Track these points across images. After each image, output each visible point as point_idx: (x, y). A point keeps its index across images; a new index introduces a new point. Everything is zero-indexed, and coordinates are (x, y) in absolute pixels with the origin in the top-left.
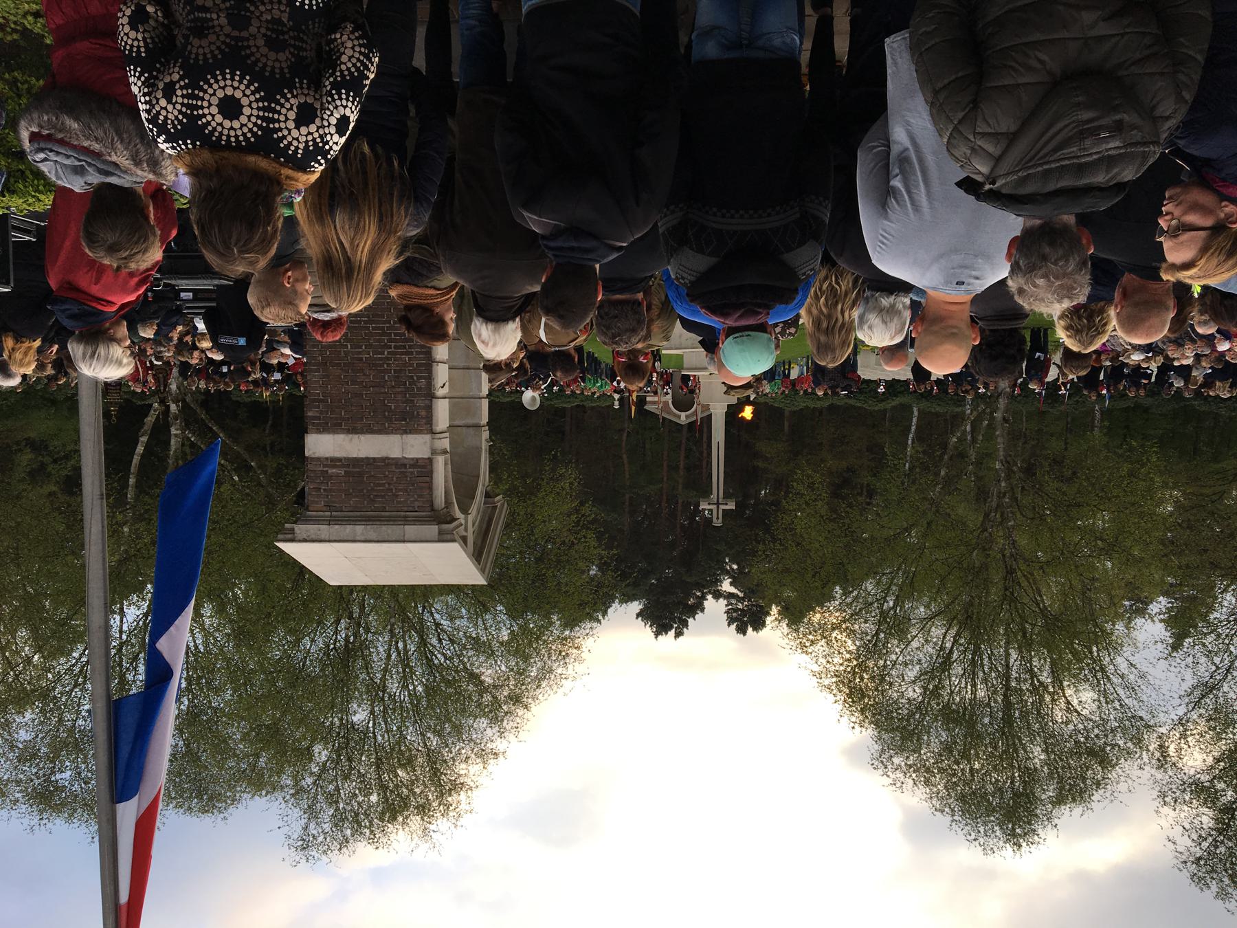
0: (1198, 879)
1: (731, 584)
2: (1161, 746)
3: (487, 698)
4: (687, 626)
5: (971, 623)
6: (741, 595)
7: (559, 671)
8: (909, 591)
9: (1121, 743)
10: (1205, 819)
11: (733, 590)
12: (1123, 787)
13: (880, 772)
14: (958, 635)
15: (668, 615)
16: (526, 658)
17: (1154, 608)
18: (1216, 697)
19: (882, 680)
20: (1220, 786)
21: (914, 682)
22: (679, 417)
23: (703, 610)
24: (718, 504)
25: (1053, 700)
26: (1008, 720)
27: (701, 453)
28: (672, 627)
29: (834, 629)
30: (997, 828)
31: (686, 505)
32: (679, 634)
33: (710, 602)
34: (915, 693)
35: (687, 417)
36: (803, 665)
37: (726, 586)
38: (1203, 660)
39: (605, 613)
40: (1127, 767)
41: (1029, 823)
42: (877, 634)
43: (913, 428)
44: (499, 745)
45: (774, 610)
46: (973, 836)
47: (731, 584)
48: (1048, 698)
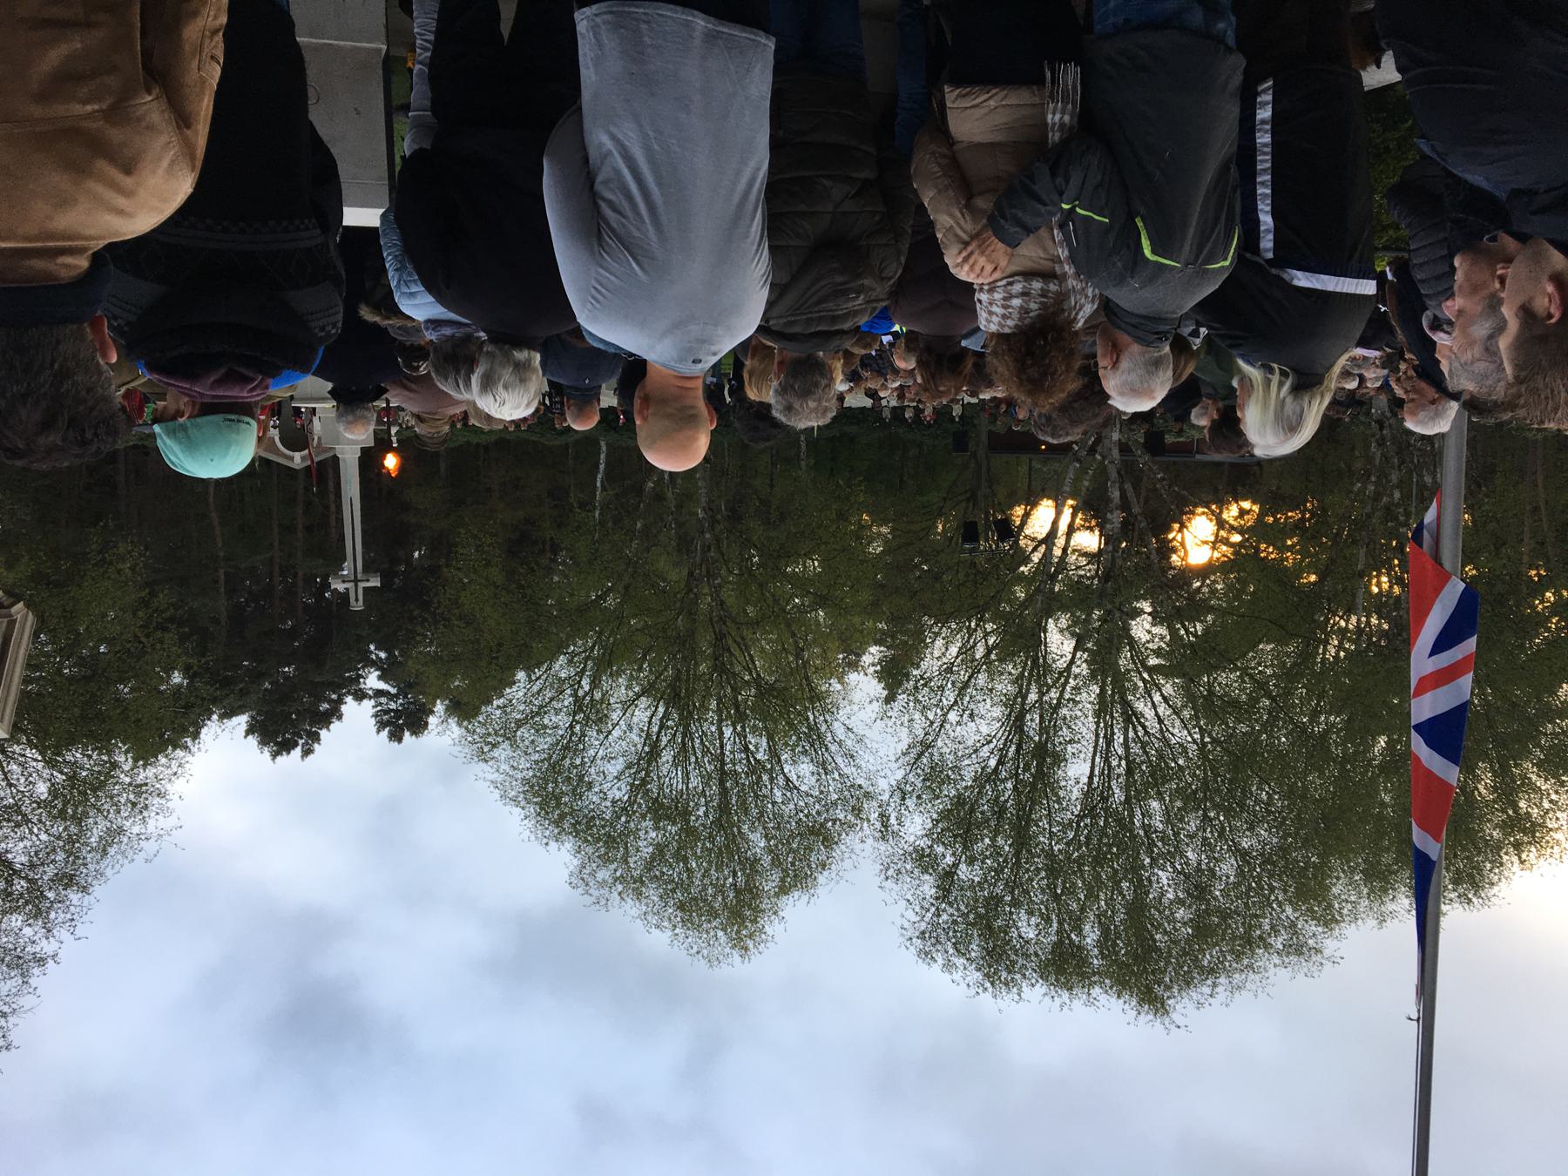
0: (925, 955)
1: (380, 678)
2: (882, 815)
3: (20, 885)
4: (318, 740)
5: (679, 698)
6: (393, 691)
7: (136, 830)
8: (605, 665)
9: (841, 816)
10: (926, 888)
11: (382, 686)
12: (848, 864)
13: (580, 890)
14: (666, 716)
15: (288, 724)
16: (78, 820)
17: (867, 659)
18: (932, 755)
19: (581, 778)
20: (940, 849)
21: (618, 778)
22: (292, 459)
23: (340, 717)
24: (356, 581)
25: (772, 779)
26: (724, 808)
27: (327, 507)
28: (296, 744)
29: (519, 727)
30: (720, 933)
31: (309, 580)
32: (307, 752)
33: (350, 706)
34: (620, 792)
35: (303, 458)
36: (481, 774)
37: (373, 681)
38: (917, 716)
39: (196, 736)
40: (850, 840)
41: (755, 921)
42: (571, 727)
43: (602, 467)
44: (46, 947)
45: (439, 707)
46: (695, 949)
47: (380, 678)
48: (765, 777)
